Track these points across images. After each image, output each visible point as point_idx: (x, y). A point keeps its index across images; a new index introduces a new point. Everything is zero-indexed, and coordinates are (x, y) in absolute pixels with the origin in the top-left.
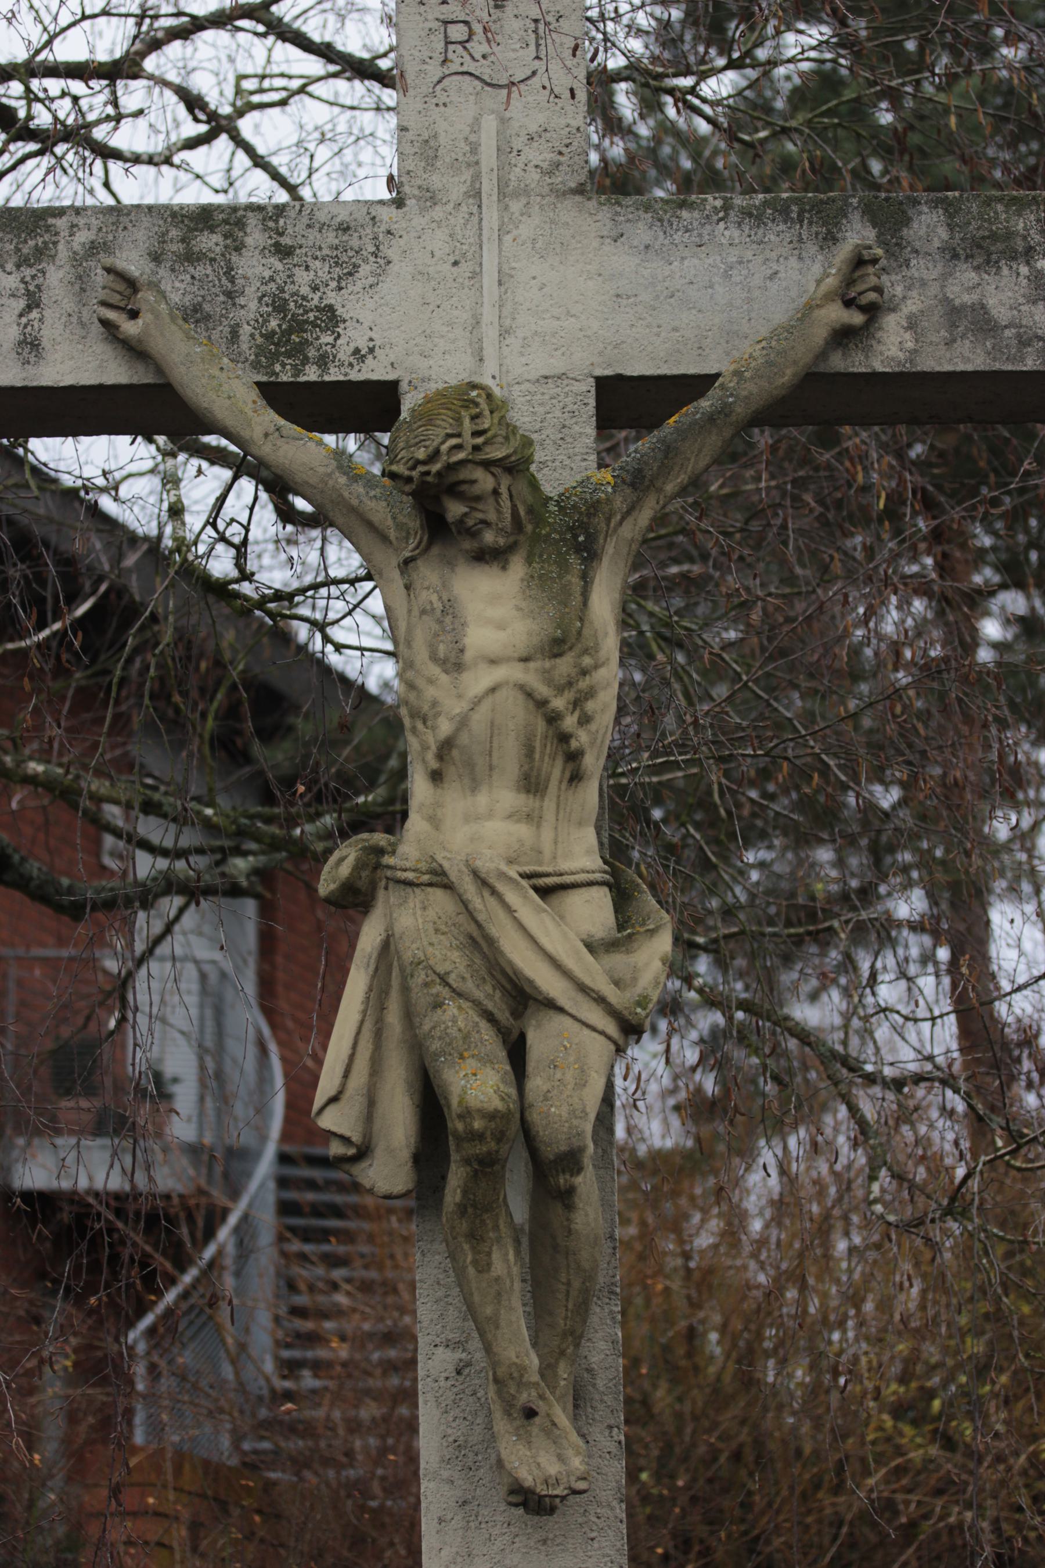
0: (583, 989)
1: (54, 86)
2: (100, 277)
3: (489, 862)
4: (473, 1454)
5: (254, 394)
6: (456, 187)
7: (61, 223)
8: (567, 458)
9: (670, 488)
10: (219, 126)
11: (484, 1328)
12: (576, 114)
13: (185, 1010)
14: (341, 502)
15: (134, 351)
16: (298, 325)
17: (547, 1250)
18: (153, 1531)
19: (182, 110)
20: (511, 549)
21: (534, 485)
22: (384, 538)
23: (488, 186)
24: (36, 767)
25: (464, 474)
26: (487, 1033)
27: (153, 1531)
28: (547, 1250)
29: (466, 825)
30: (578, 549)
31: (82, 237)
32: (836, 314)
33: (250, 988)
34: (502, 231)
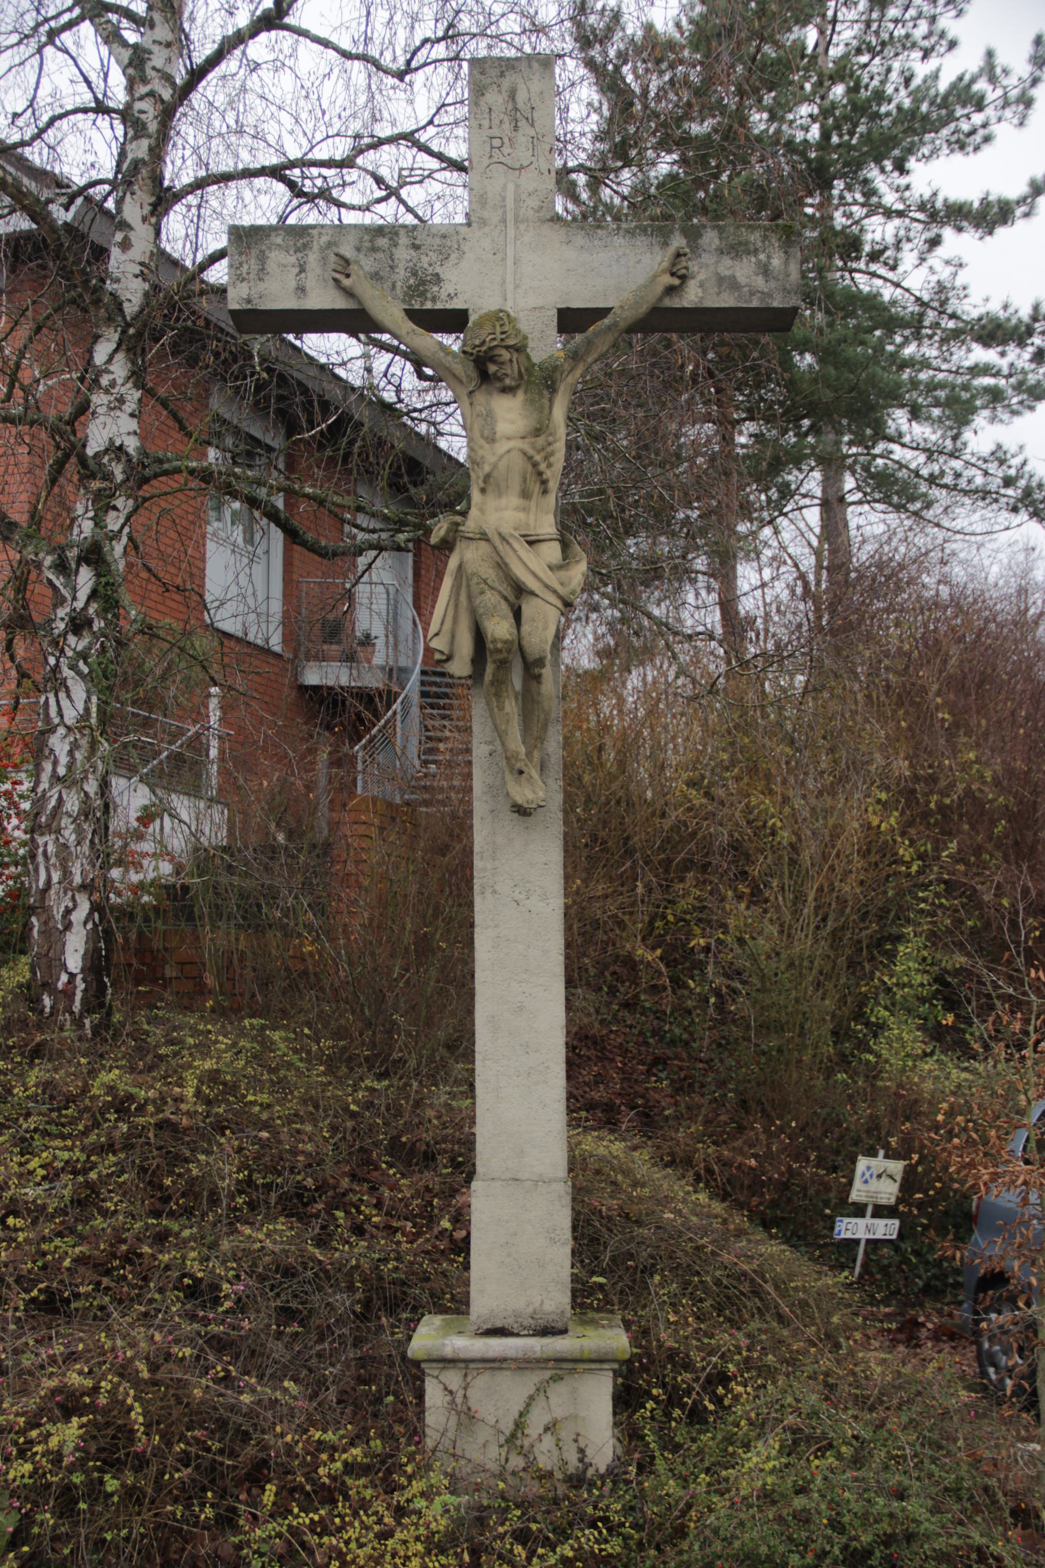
0: (547, 586)
1: (314, 171)
2: (332, 258)
3: (505, 530)
4: (497, 790)
5: (403, 314)
6: (495, 218)
7: (315, 232)
8: (546, 345)
9: (590, 360)
10: (392, 193)
11: (501, 735)
12: (551, 182)
13: (380, 604)
14: (448, 370)
15: (349, 293)
16: (423, 282)
17: (529, 700)
18: (362, 829)
19: (375, 186)
20: (518, 387)
21: (528, 358)
22: (461, 382)
23: (510, 217)
24: (309, 490)
25: (497, 352)
26: (504, 606)
27: (362, 829)
28: (529, 700)
29: (496, 512)
30: (548, 387)
31: (325, 239)
32: (668, 280)
33: (410, 599)
34: (516, 238)
